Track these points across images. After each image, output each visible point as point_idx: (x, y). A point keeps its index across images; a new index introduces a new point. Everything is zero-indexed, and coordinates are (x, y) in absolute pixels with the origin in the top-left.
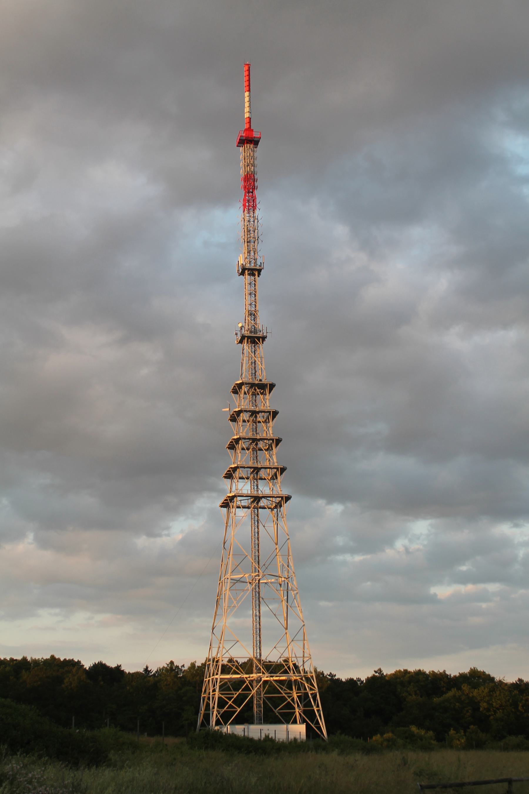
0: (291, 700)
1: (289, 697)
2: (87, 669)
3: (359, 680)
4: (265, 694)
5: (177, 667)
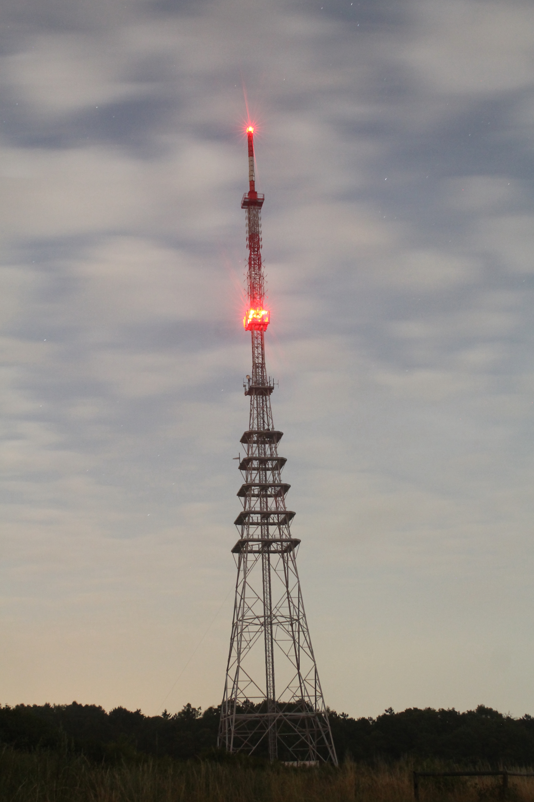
0: (305, 738)
1: (303, 735)
2: (108, 713)
3: (371, 719)
4: (280, 733)
5: (194, 709)
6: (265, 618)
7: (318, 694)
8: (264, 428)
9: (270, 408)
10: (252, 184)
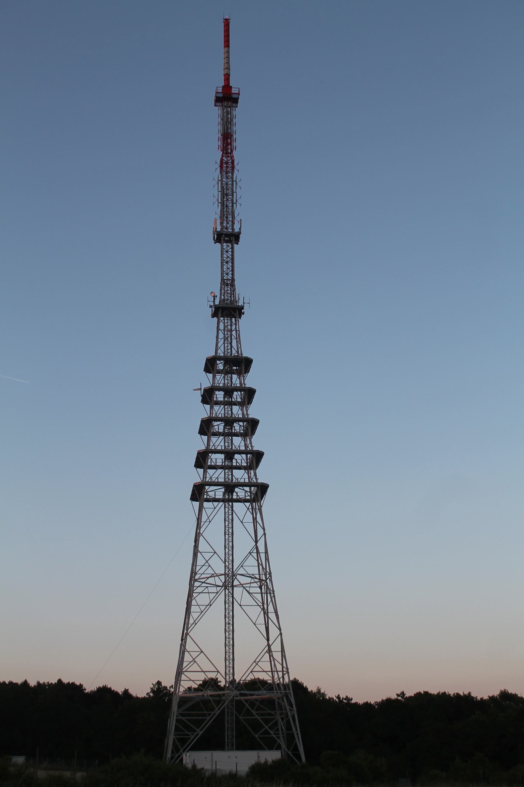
2: (121, 693)
5: (165, 688)
7: (285, 670)
9: (239, 331)
10: (227, 77)
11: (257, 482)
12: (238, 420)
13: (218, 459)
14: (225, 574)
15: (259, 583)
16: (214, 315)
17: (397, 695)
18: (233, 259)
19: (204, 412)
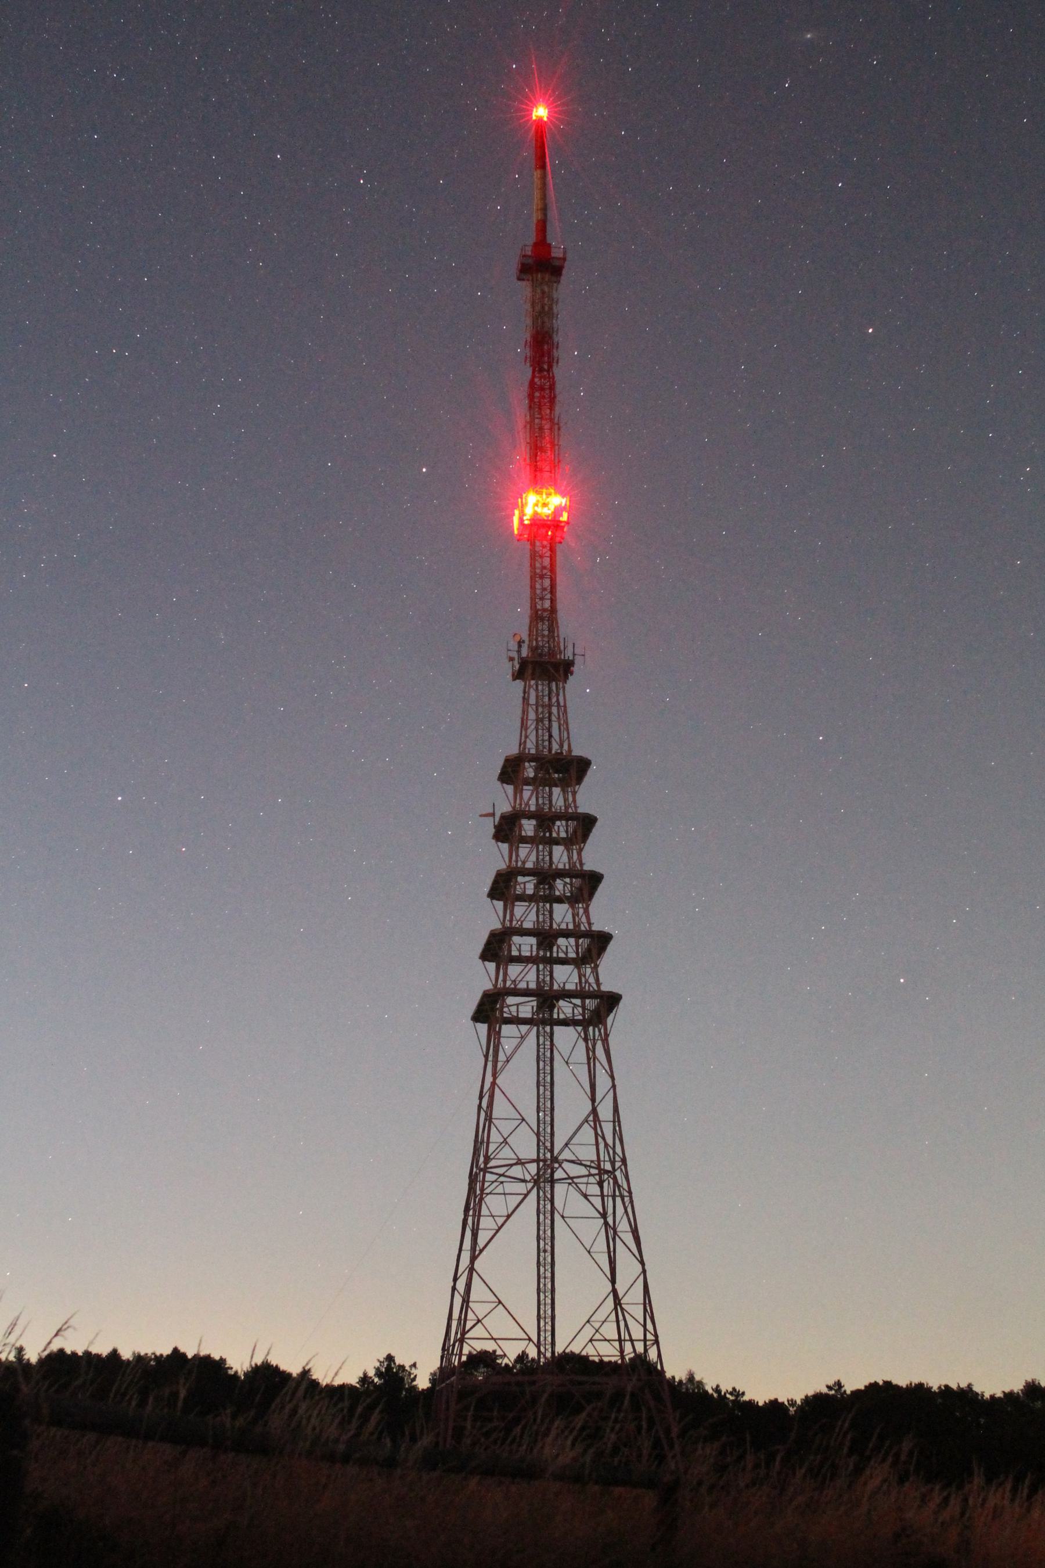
5: (402, 1367)
6: (538, 1165)
7: (649, 1337)
8: (550, 750)
9: (565, 706)
10: (542, 227)
11: (591, 931)
12: (561, 874)
13: (526, 945)
14: (537, 1161)
15: (597, 1177)
16: (519, 675)
17: (828, 1387)
18: (552, 570)
19: (496, 857)
